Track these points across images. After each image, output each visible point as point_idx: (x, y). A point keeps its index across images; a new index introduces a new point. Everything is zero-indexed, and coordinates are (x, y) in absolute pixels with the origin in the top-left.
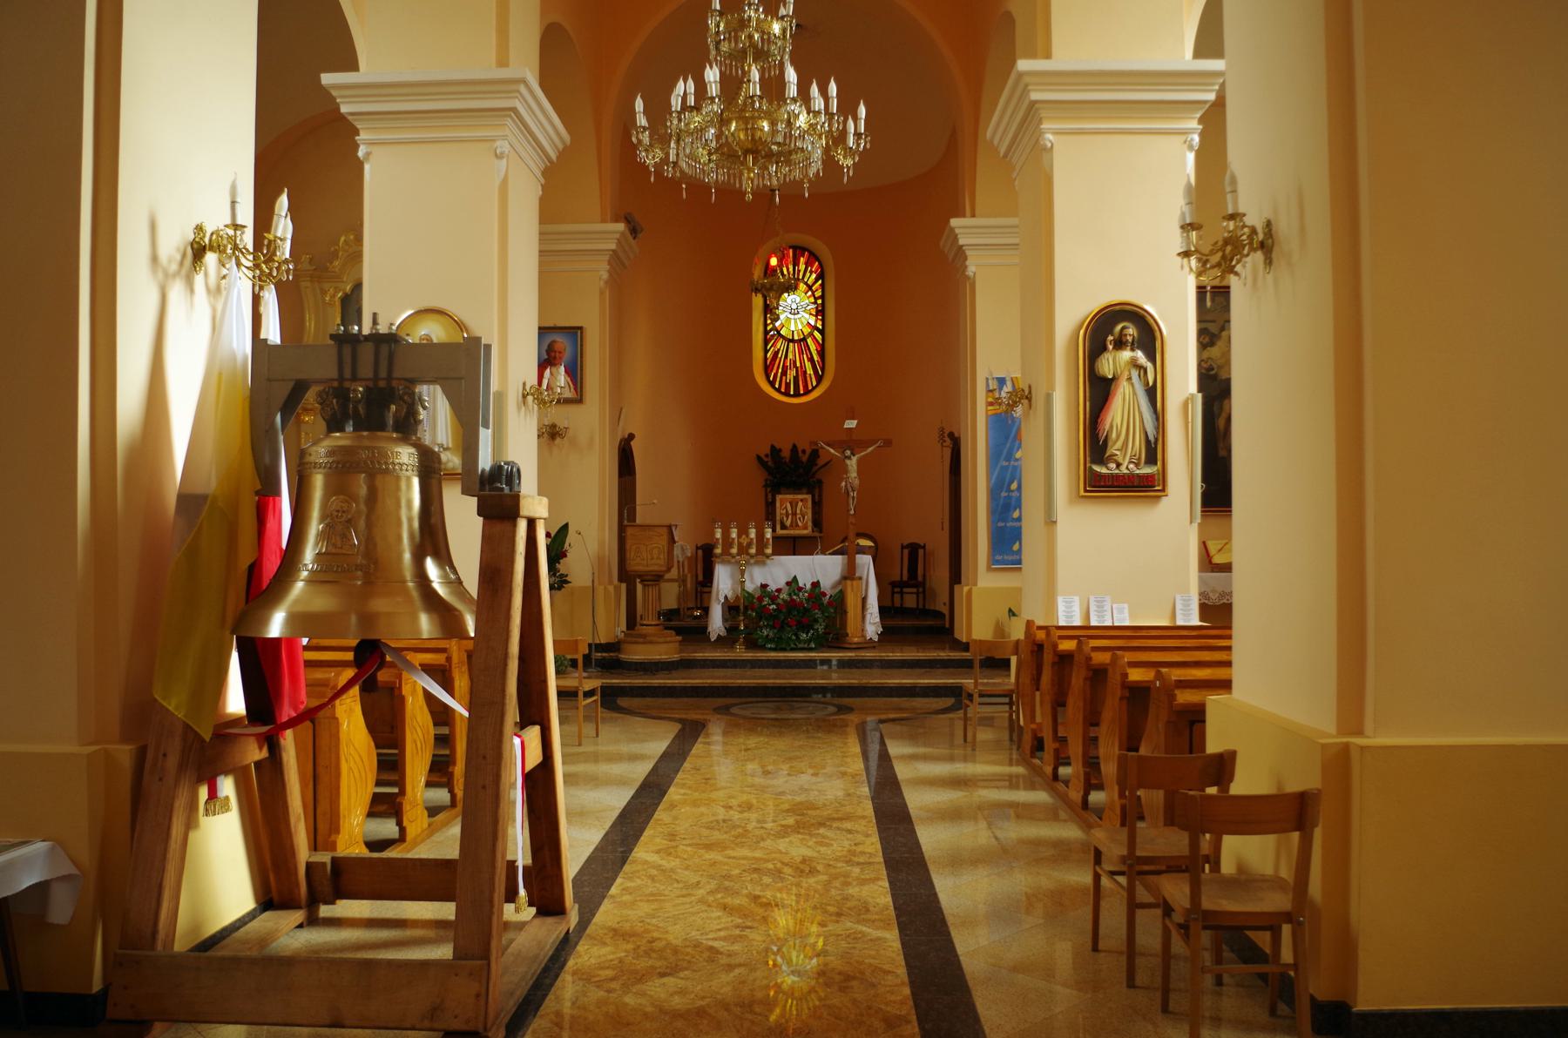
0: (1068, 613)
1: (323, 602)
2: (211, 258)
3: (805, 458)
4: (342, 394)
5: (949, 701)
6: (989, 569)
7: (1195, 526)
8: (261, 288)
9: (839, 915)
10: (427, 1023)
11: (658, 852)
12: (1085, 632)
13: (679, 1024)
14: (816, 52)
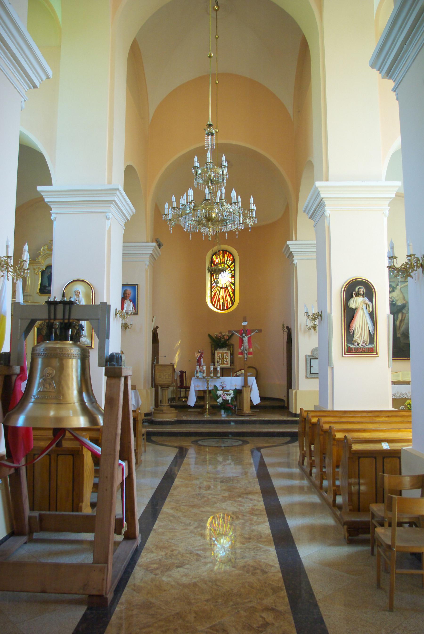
4: (50, 326)
5: (289, 439)
8: (17, 280)
11: (172, 509)
13: (186, 590)
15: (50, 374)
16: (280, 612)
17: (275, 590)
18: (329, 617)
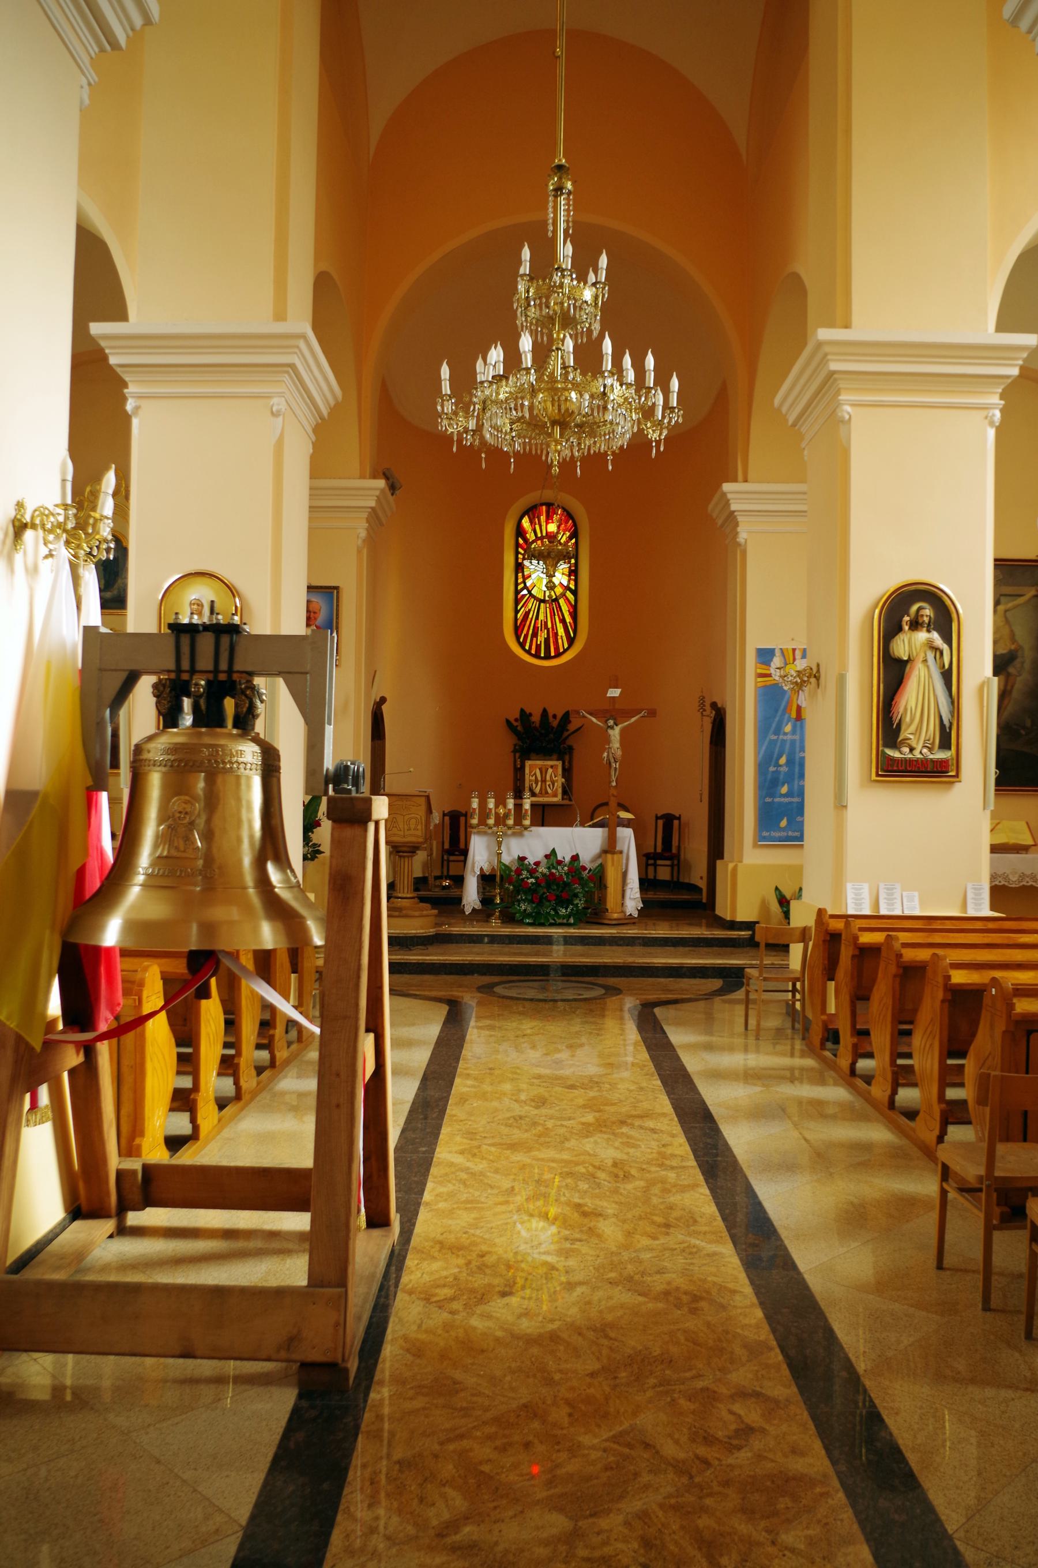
0: (856, 901)
1: (158, 910)
2: (29, 535)
3: (555, 723)
5: (717, 983)
6: (755, 846)
7: (988, 813)
9: (667, 1226)
10: (283, 1354)
12: (876, 921)
13: (535, 1350)
14: (630, 320)
15: (186, 813)
16: (776, 1402)
17: (754, 1350)
18: (897, 1414)
